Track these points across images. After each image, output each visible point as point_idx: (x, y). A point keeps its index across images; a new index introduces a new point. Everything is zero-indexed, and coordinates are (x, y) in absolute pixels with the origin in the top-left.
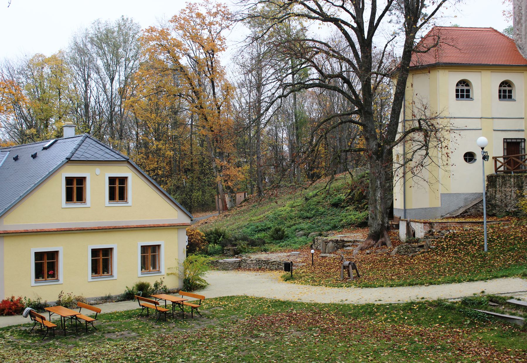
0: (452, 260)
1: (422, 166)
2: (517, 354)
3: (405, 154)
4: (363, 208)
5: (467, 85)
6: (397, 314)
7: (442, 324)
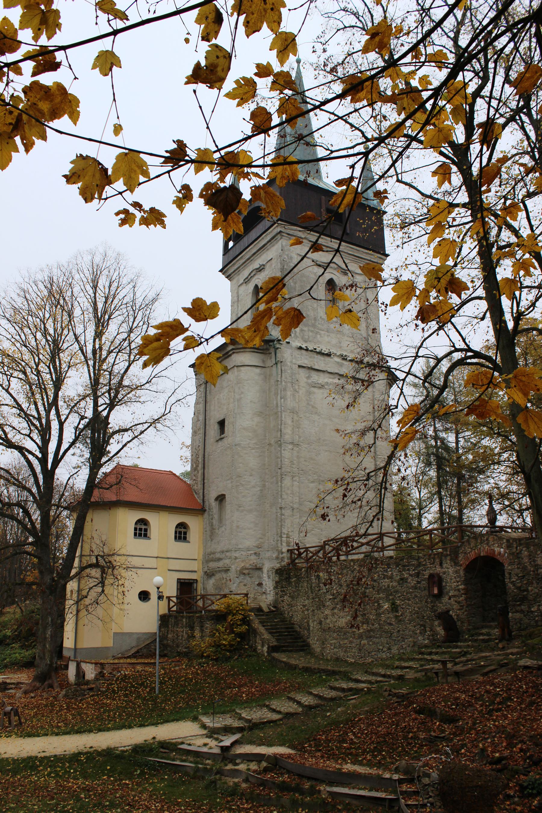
0: (123, 704)
1: (97, 603)
2: (188, 805)
3: (79, 591)
4: (30, 646)
5: (185, 528)
6: (61, 767)
7: (111, 776)
